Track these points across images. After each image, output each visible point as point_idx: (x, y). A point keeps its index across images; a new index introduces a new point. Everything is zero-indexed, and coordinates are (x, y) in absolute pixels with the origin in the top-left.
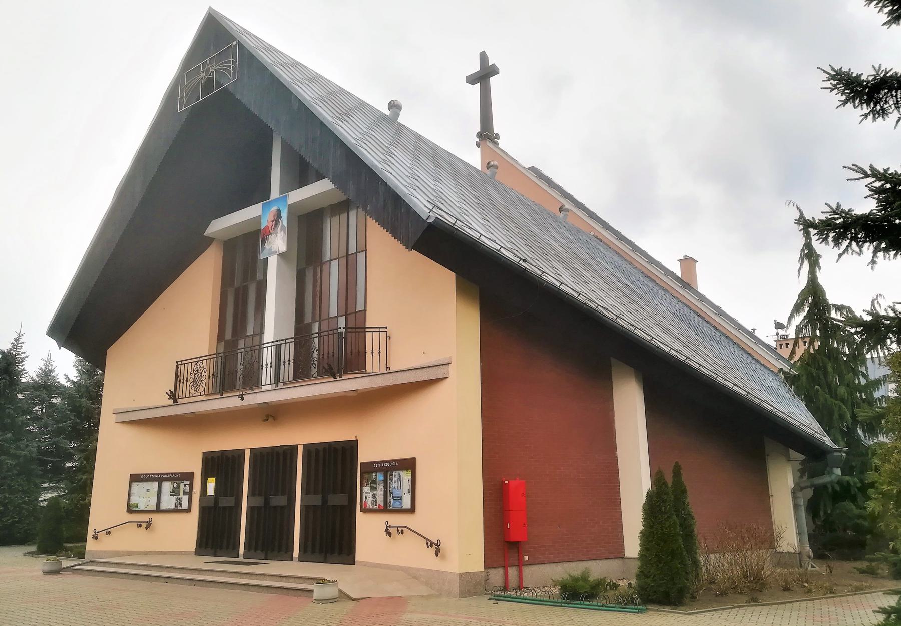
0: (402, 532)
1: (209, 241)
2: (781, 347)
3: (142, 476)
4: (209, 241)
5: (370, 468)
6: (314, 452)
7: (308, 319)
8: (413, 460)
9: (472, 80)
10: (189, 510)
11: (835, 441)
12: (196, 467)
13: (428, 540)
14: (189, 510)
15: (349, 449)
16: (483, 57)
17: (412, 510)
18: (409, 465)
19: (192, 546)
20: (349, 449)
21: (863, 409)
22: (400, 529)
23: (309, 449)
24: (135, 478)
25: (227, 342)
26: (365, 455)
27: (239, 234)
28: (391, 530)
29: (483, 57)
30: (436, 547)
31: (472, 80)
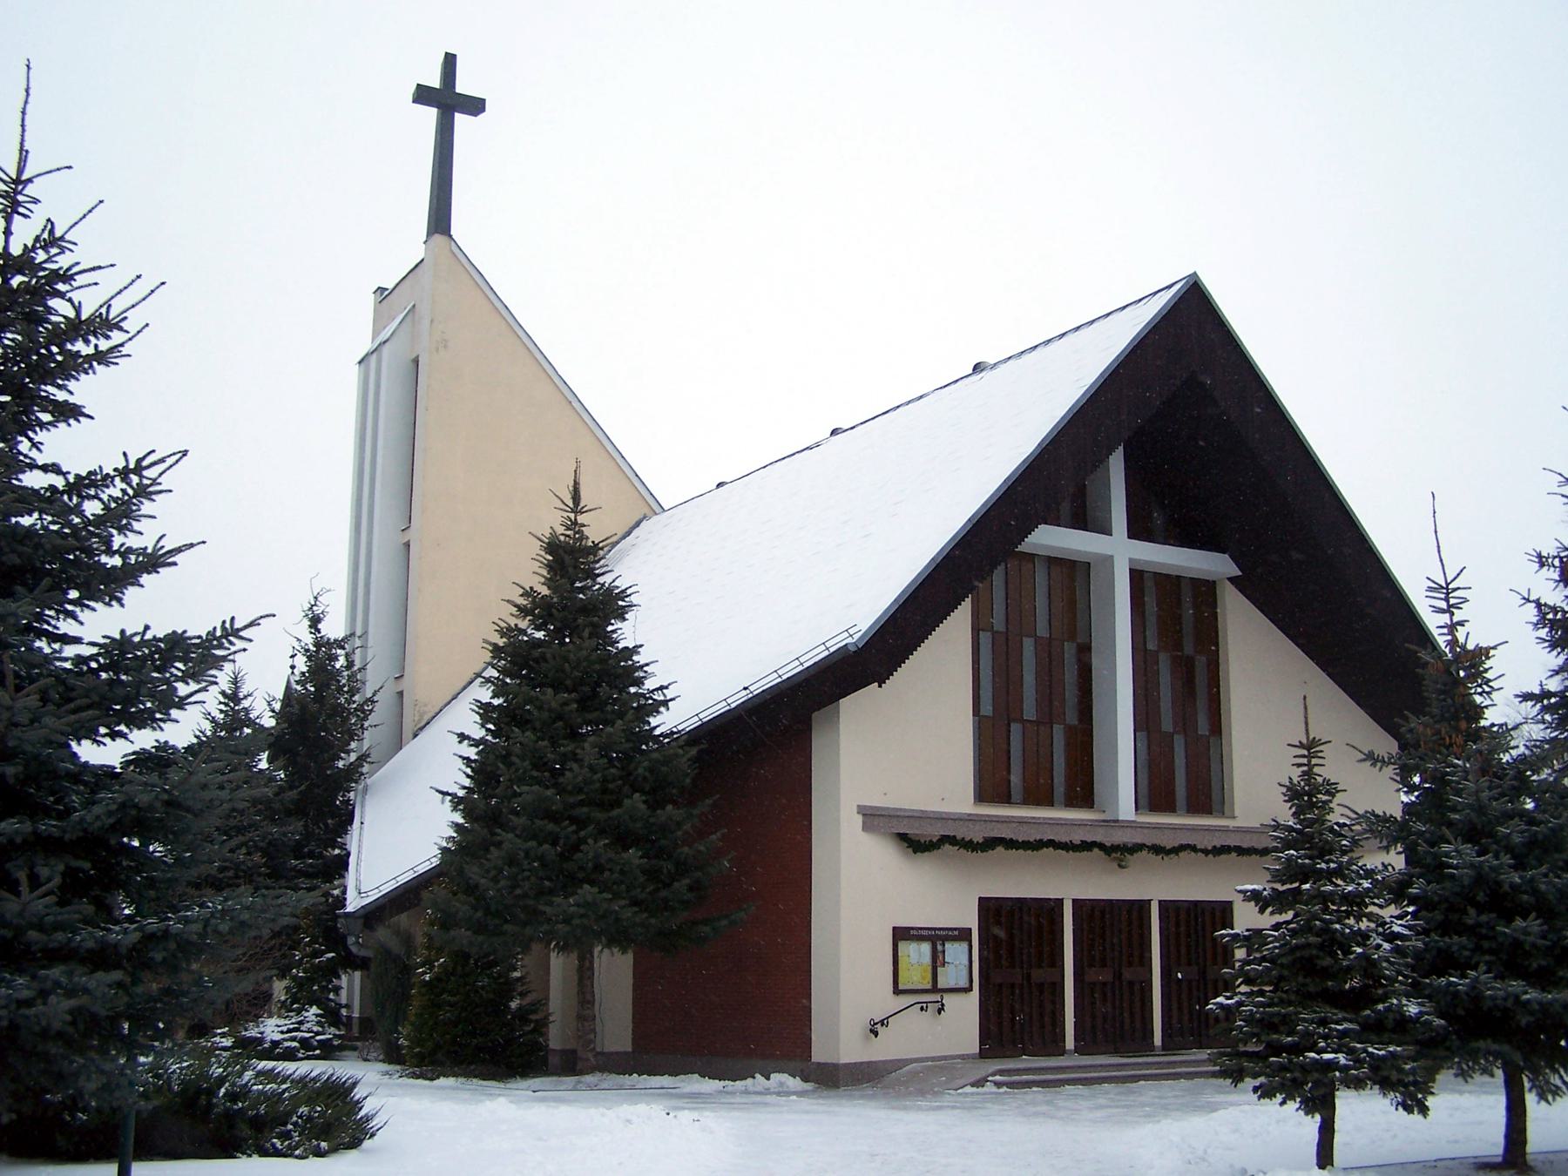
12: (971, 921)
14: (970, 989)
23: (1163, 905)
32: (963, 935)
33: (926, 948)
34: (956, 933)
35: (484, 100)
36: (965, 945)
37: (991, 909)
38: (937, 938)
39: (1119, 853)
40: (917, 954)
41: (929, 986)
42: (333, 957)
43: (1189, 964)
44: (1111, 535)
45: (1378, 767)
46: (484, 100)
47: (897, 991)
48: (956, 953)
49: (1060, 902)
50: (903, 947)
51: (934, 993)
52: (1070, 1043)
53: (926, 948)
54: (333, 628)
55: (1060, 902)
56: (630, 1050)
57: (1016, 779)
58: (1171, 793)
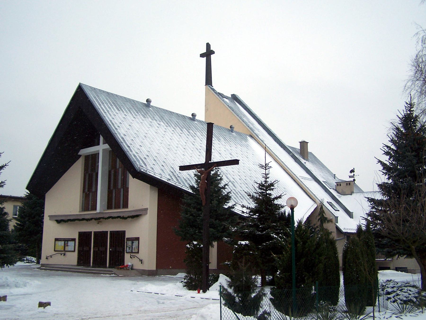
0: (134, 257)
1: (80, 156)
2: (338, 186)
3: (59, 239)
4: (80, 156)
5: (128, 239)
6: (113, 233)
7: (112, 188)
8: (139, 238)
9: (202, 55)
10: (74, 251)
11: (273, 236)
12: (76, 237)
13: (140, 259)
14: (74, 251)
15: (123, 233)
16: (208, 45)
17: (138, 252)
18: (138, 239)
19: (76, 263)
20: (123, 233)
21: (7, 254)
22: (134, 256)
23: (111, 232)
24: (57, 240)
25: (86, 194)
26: (127, 236)
27: (91, 154)
28: (131, 256)
29: (208, 45)
30: (141, 261)
31: (202, 55)
32: (74, 240)
33: (63, 242)
34: (71, 239)
35: (200, 57)
36: (74, 242)
37: (81, 235)
38: (66, 241)
39: (98, 220)
40: (61, 244)
41: (63, 250)
42: (246, 245)
43: (113, 247)
44: (99, 150)
45: (390, 144)
46: (200, 57)
47: (55, 251)
48: (71, 244)
49: (107, 232)
50: (57, 242)
51: (64, 252)
52: (108, 266)
53: (63, 242)
54: (195, 173)
55: (107, 232)
56: (216, 268)
57: (90, 207)
58: (111, 204)
